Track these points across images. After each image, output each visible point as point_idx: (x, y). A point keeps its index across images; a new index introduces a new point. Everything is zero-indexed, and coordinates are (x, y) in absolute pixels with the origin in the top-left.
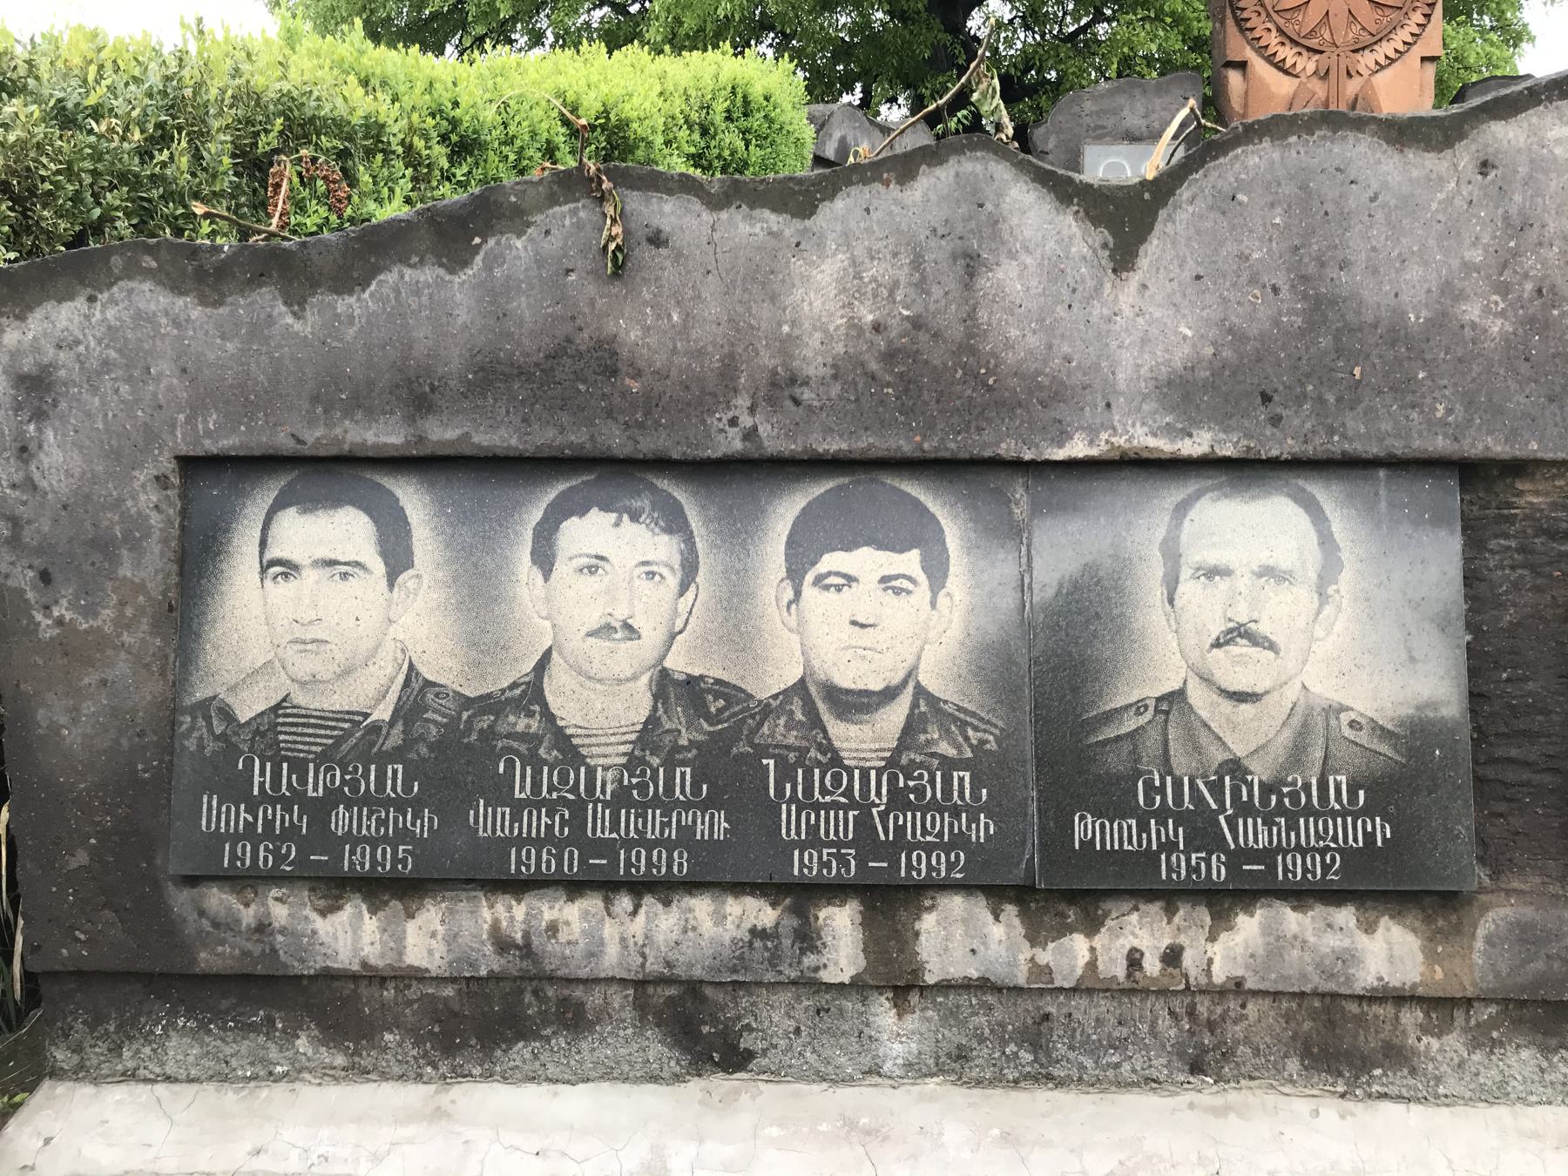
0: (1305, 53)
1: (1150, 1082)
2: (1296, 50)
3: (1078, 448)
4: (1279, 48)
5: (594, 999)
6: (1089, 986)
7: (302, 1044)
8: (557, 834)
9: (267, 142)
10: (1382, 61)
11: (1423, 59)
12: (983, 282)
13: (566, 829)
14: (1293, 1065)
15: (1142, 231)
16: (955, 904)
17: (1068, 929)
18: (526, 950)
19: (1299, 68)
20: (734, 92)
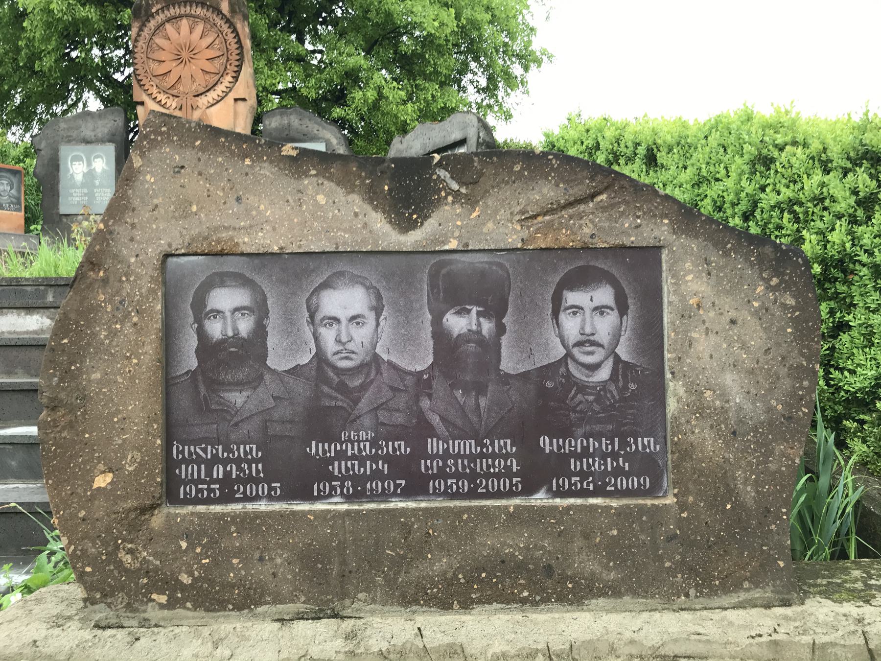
0: (171, 97)
2: (166, 96)
4: (158, 95)
8: (514, 460)
11: (236, 100)
13: (408, 449)
19: (168, 105)
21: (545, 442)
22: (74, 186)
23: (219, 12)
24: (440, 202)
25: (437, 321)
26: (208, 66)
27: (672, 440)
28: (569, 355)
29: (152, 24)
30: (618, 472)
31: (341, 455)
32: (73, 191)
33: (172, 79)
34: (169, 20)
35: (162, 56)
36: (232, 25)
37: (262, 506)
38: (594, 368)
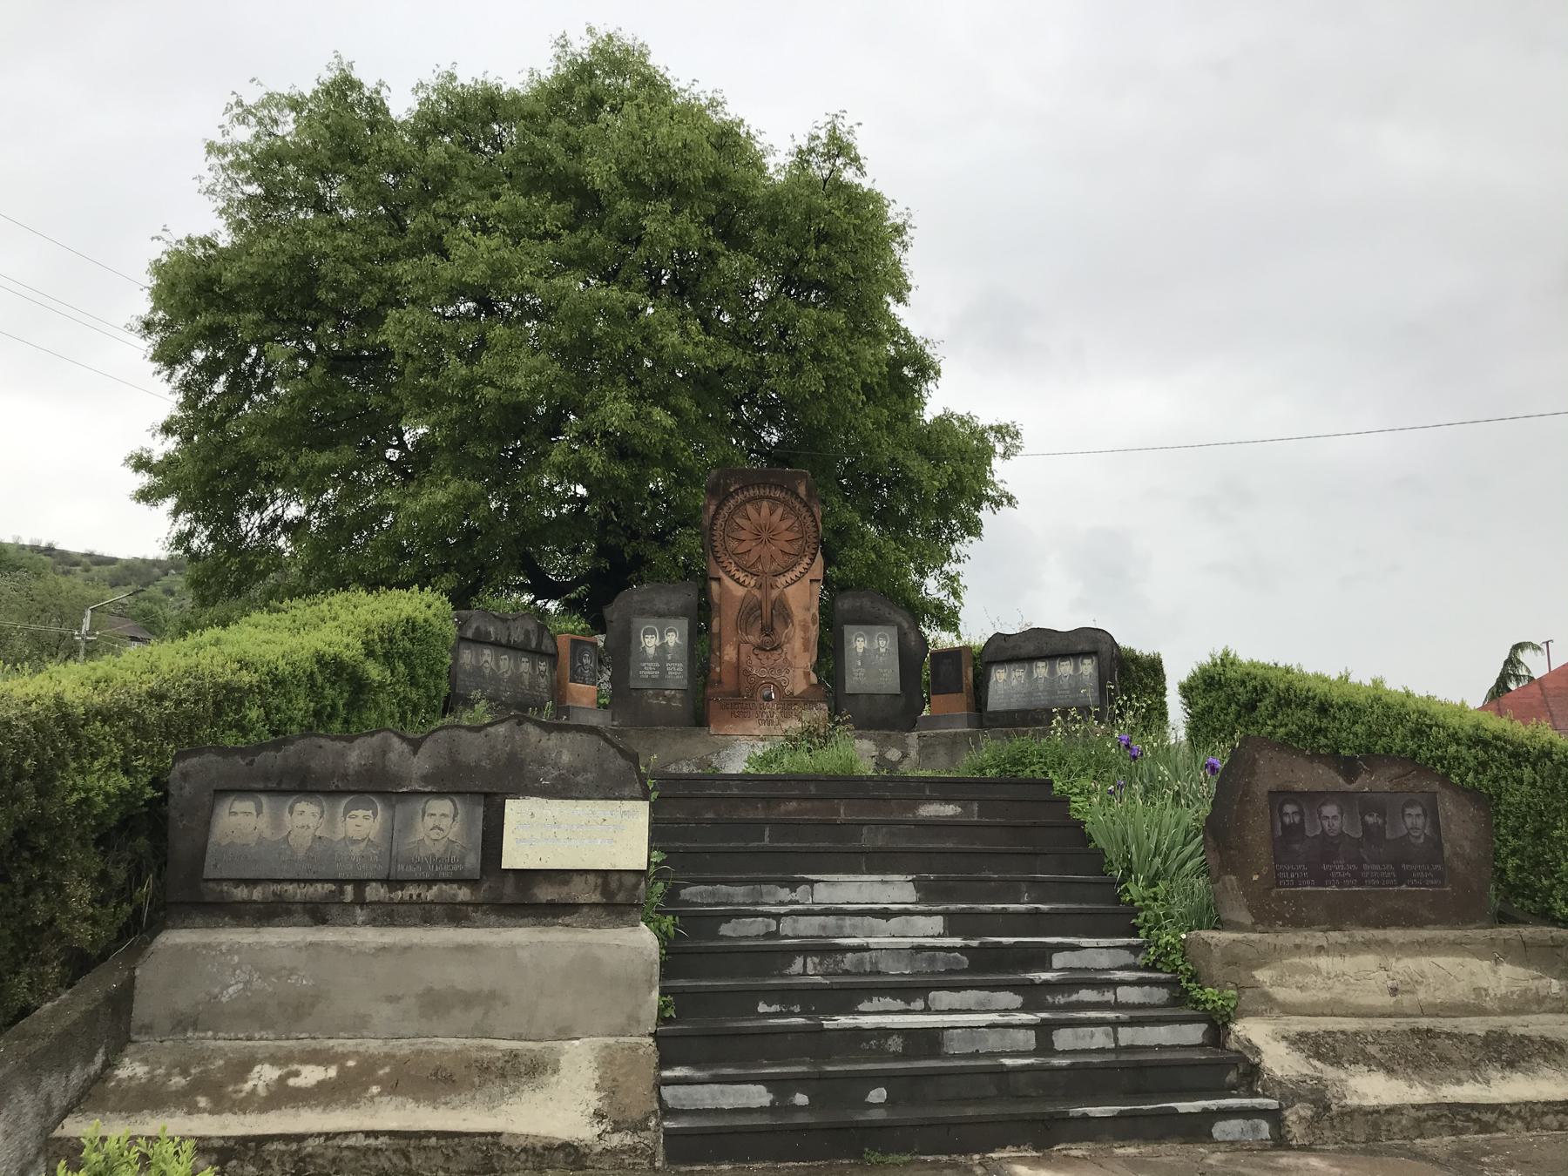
1: (415, 925)
3: (405, 790)
5: (294, 908)
6: (402, 902)
7: (226, 919)
9: (220, 697)
10: (789, 581)
11: (811, 581)
12: (387, 757)
14: (446, 920)
15: (420, 747)
16: (374, 884)
17: (397, 890)
18: (280, 895)
19: (746, 583)
20: (407, 622)
21: (1403, 866)
22: (646, 660)
23: (798, 496)
24: (1361, 773)
25: (1363, 818)
26: (787, 548)
27: (897, 1057)
28: (1409, 833)
29: (732, 503)
30: (1430, 878)
31: (1334, 870)
32: (644, 664)
33: (753, 558)
34: (749, 500)
35: (743, 535)
36: (810, 509)
37: (1309, 888)
38: (1418, 837)
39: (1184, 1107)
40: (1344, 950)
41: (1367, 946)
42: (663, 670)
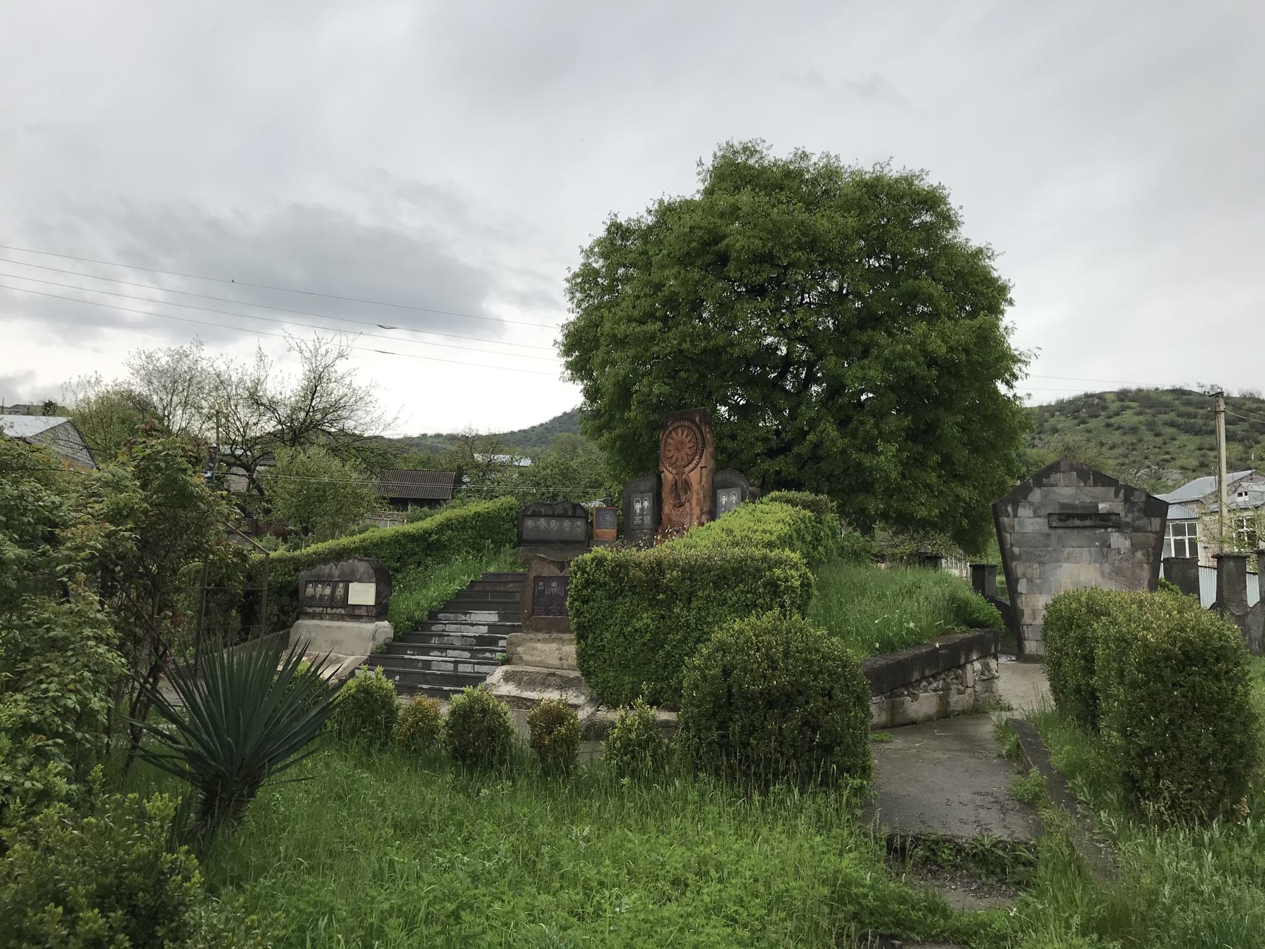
35: (670, 448)
39: (445, 688)
40: (545, 641)
41: (554, 640)
42: (642, 519)
